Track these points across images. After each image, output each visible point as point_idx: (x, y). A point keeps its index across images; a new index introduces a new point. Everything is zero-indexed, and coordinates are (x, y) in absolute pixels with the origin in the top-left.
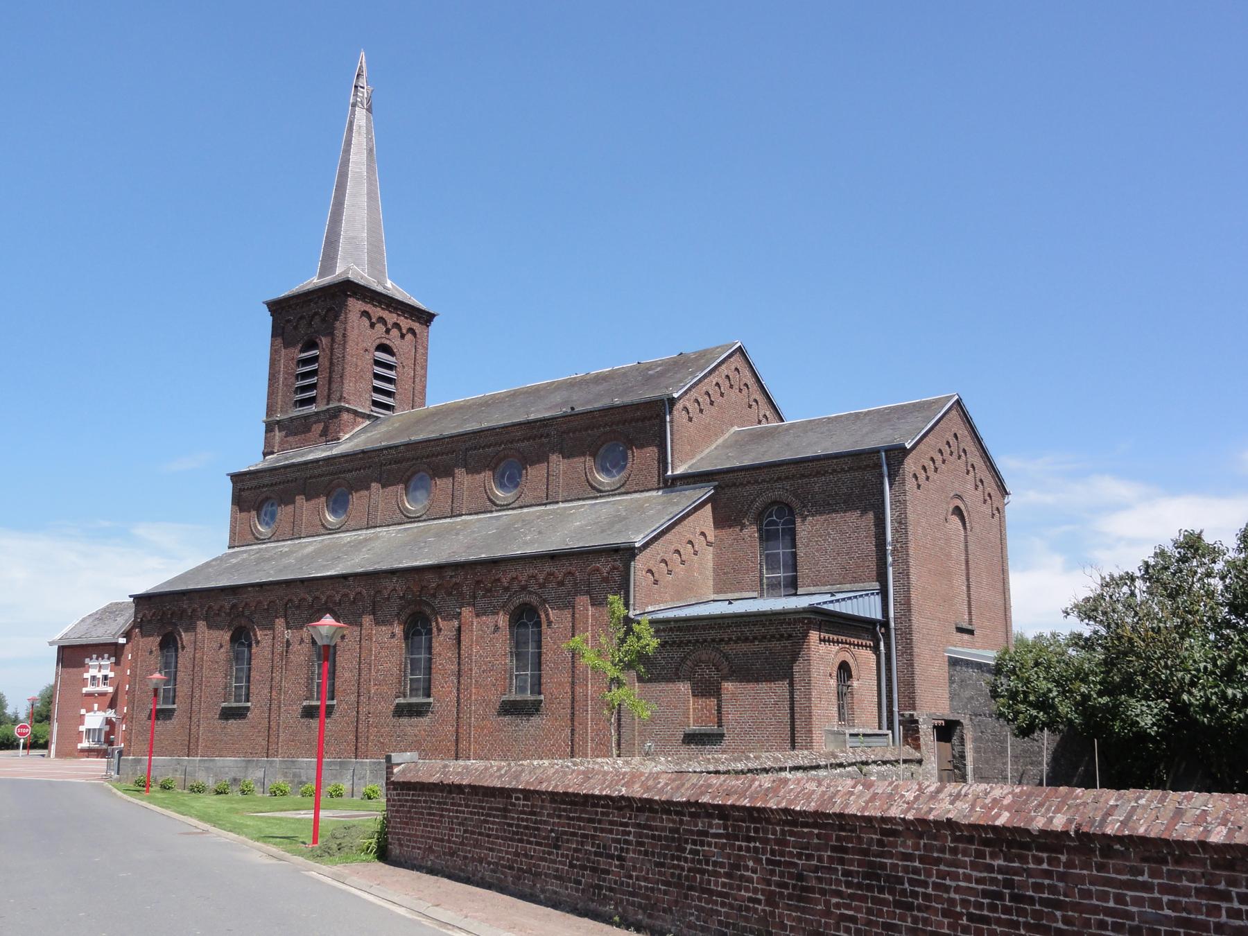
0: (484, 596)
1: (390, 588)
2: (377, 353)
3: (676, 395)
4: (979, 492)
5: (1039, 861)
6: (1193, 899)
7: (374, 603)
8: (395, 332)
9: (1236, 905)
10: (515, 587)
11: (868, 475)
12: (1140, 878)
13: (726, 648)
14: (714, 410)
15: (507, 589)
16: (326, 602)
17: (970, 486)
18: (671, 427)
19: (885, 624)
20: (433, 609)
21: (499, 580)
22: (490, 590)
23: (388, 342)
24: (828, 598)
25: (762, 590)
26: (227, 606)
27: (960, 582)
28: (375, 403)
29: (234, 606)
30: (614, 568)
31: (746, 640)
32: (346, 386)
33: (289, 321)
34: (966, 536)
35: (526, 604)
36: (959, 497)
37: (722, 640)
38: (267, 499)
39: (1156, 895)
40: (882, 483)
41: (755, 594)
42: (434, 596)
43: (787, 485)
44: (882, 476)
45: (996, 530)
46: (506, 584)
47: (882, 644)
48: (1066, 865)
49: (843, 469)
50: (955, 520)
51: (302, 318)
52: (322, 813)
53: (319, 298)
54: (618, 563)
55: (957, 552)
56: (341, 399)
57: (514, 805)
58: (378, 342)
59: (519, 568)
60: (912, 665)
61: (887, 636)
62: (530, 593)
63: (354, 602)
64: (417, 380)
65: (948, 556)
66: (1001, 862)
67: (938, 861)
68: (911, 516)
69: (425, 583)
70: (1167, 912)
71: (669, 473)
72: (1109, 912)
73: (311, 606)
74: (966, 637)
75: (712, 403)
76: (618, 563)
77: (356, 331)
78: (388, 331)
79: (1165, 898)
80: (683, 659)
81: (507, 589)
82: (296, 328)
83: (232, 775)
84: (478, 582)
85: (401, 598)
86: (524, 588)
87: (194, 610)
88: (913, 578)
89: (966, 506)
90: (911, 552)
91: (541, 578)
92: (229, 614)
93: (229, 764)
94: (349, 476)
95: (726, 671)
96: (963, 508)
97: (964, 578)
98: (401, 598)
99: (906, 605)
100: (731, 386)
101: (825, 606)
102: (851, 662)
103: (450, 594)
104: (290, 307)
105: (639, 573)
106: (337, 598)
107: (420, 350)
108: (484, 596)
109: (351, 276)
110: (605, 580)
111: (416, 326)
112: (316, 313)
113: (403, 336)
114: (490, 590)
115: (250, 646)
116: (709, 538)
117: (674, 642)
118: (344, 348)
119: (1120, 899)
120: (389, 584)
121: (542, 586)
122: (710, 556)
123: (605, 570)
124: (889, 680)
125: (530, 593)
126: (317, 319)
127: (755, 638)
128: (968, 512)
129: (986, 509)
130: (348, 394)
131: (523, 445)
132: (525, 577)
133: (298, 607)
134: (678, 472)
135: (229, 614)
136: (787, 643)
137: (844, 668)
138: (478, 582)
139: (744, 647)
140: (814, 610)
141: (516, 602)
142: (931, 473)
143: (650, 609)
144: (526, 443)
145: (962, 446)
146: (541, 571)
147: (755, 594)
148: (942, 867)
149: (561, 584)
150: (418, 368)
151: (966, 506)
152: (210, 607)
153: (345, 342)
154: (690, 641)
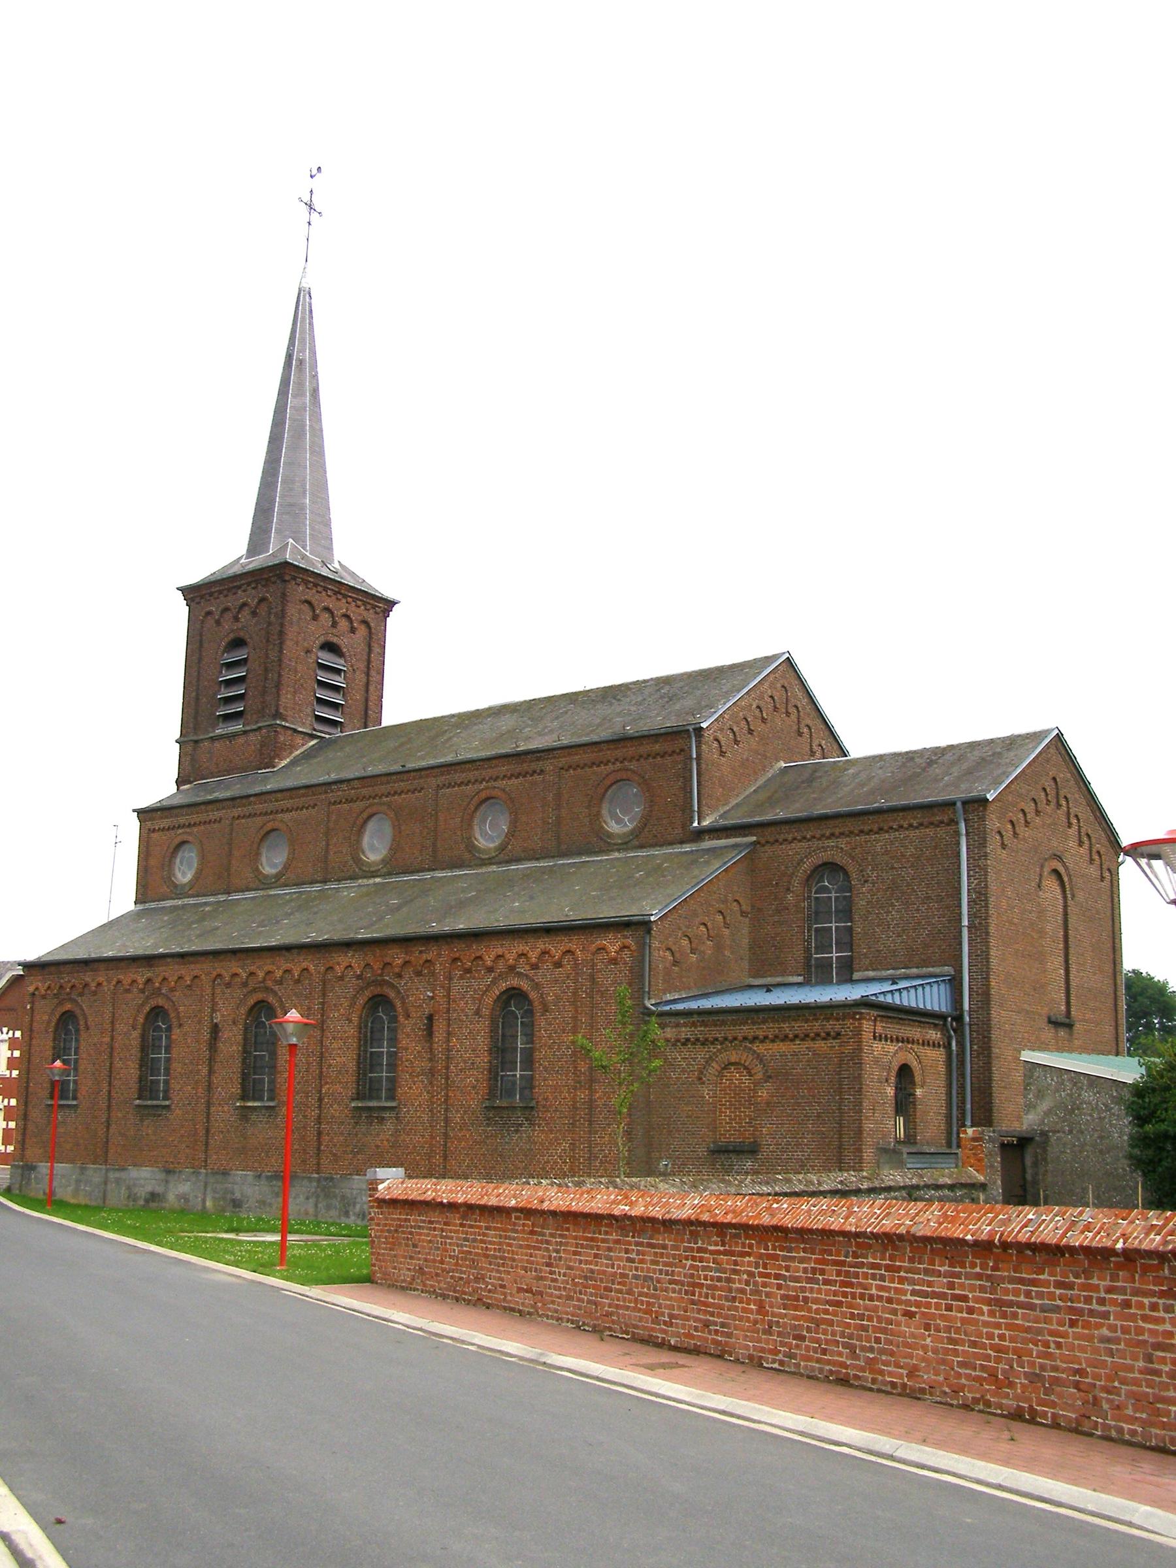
0: (461, 977)
1: (345, 964)
2: (320, 654)
3: (704, 725)
4: (1083, 851)
5: (973, 1265)
6: (1076, 1292)
7: (324, 982)
8: (343, 624)
9: (1103, 1295)
10: (501, 966)
11: (941, 832)
12: (1041, 1277)
13: (759, 1048)
14: (753, 741)
15: (490, 970)
16: (264, 980)
17: (1072, 844)
18: (698, 765)
19: (959, 1019)
20: (399, 992)
21: (480, 958)
22: (468, 971)
23: (335, 640)
24: (887, 987)
25: (809, 972)
26: (141, 980)
27: (1055, 963)
28: (320, 719)
29: (149, 980)
30: (624, 947)
31: (786, 1038)
32: (283, 700)
33: (209, 613)
34: (1065, 907)
35: (514, 988)
36: (1059, 858)
37: (755, 1038)
38: (183, 843)
39: (1052, 1289)
40: (958, 844)
41: (800, 979)
42: (399, 976)
43: (842, 843)
44: (957, 833)
45: (1106, 897)
46: (489, 963)
47: (954, 1044)
48: (993, 1269)
49: (911, 825)
50: (1051, 884)
51: (227, 609)
52: (290, 1237)
53: (249, 584)
54: (629, 941)
55: (1053, 927)
56: (277, 715)
57: (515, 1224)
58: (322, 639)
59: (506, 943)
60: (989, 1070)
61: (959, 1031)
62: (519, 974)
63: (298, 981)
64: (372, 688)
65: (1042, 933)
66: (946, 1268)
67: (899, 1269)
68: (993, 887)
69: (388, 960)
70: (1059, 1303)
71: (696, 824)
72: (1020, 1305)
73: (245, 984)
74: (1062, 1033)
75: (750, 732)
76: (629, 941)
77: (295, 628)
78: (334, 624)
79: (1058, 1292)
80: (709, 1061)
81: (490, 970)
82: (218, 622)
83: (149, 1189)
84: (455, 960)
85: (359, 977)
86: (512, 968)
87: (99, 984)
88: (994, 961)
89: (1066, 868)
90: (992, 929)
91: (533, 956)
92: (142, 991)
93: (145, 1178)
94: (287, 816)
95: (760, 1076)
96: (1062, 870)
97: (1061, 959)
98: (359, 977)
99: (983, 997)
100: (775, 709)
101: (881, 998)
102: (914, 1064)
103: (419, 974)
104: (211, 594)
105: (655, 953)
106: (278, 974)
107: (376, 649)
108: (461, 977)
109: (288, 557)
110: (614, 961)
111: (370, 616)
112: (244, 605)
113: (353, 630)
114: (468, 971)
115: (169, 1029)
116: (744, 907)
117: (697, 1040)
118: (281, 651)
119: (1028, 1294)
120: (341, 960)
121: (535, 967)
122: (745, 931)
123: (613, 949)
124: (962, 1087)
125: (519, 974)
126: (246, 612)
127: (796, 1036)
128: (1069, 876)
129: (1093, 871)
130: (286, 708)
131: (510, 782)
132: (514, 955)
133: (228, 985)
134: (705, 823)
135: (142, 991)
136: (835, 1043)
137: (905, 1072)
138: (455, 960)
139: (783, 1047)
140: (865, 1003)
141: (504, 986)
142: (1021, 829)
143: (669, 997)
144: (514, 781)
145: (1062, 793)
146: (533, 948)
147: (800, 979)
148: (902, 1274)
149: (558, 965)
150: (373, 673)
151: (1066, 868)
152: (119, 982)
153: (281, 643)
154: (716, 1039)
